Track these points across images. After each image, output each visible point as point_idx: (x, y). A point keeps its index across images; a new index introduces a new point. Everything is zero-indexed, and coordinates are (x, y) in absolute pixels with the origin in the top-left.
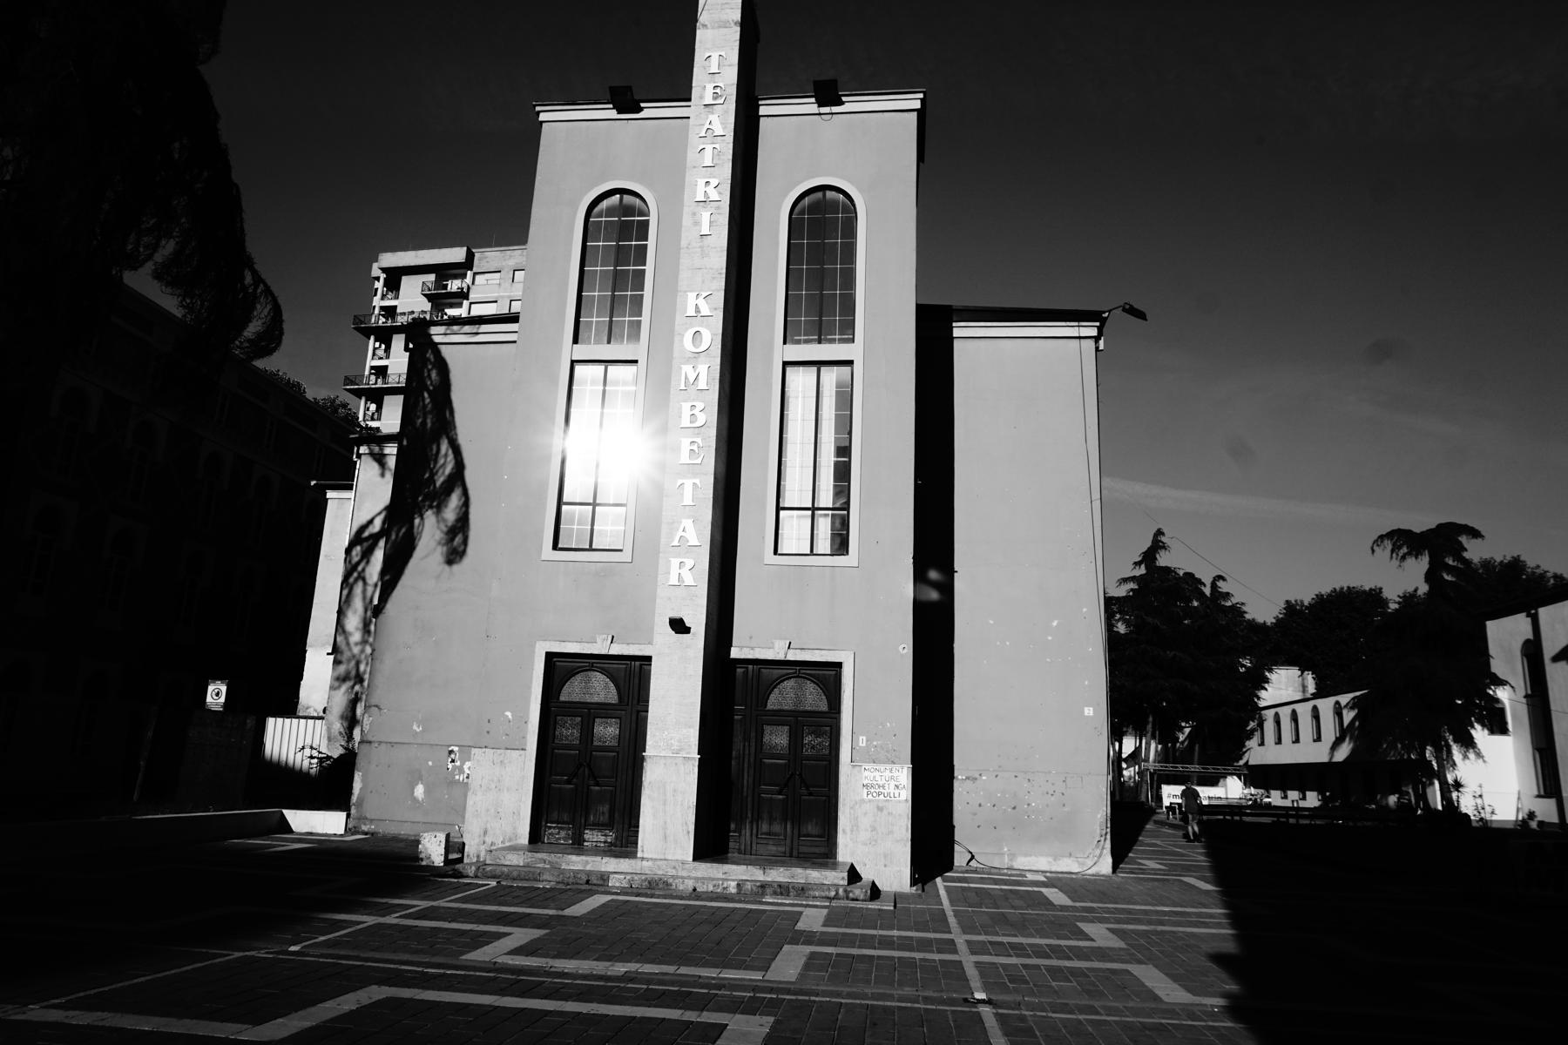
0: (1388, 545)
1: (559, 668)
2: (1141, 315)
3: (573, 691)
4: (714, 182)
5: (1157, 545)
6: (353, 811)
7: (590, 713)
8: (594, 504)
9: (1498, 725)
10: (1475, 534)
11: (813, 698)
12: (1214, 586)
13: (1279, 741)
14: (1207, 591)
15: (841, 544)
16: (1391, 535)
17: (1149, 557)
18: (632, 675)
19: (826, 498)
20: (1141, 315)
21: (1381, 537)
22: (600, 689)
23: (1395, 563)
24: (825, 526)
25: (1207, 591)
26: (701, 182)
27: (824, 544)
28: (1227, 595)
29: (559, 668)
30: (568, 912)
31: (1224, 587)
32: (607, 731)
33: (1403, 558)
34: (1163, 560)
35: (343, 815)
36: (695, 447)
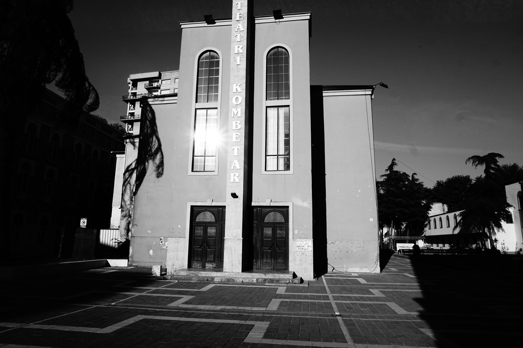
0: (472, 161)
1: (195, 211)
2: (386, 86)
3: (200, 218)
4: (241, 47)
5: (393, 164)
6: (130, 259)
7: (206, 225)
8: (278, 155)
9: (509, 220)
10: (501, 156)
11: (279, 218)
12: (413, 177)
13: (436, 228)
14: (410, 178)
15: (287, 167)
16: (472, 158)
17: (391, 168)
18: (220, 212)
19: (282, 152)
20: (386, 86)
21: (469, 158)
22: (209, 217)
23: (474, 167)
24: (282, 161)
25: (410, 178)
26: (236, 47)
27: (282, 167)
28: (417, 180)
29: (195, 211)
30: (214, 285)
31: (416, 177)
32: (212, 231)
33: (477, 165)
34: (395, 168)
35: (127, 260)
36: (237, 136)
